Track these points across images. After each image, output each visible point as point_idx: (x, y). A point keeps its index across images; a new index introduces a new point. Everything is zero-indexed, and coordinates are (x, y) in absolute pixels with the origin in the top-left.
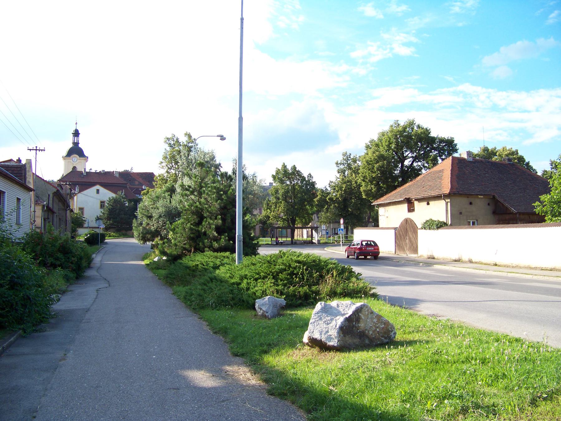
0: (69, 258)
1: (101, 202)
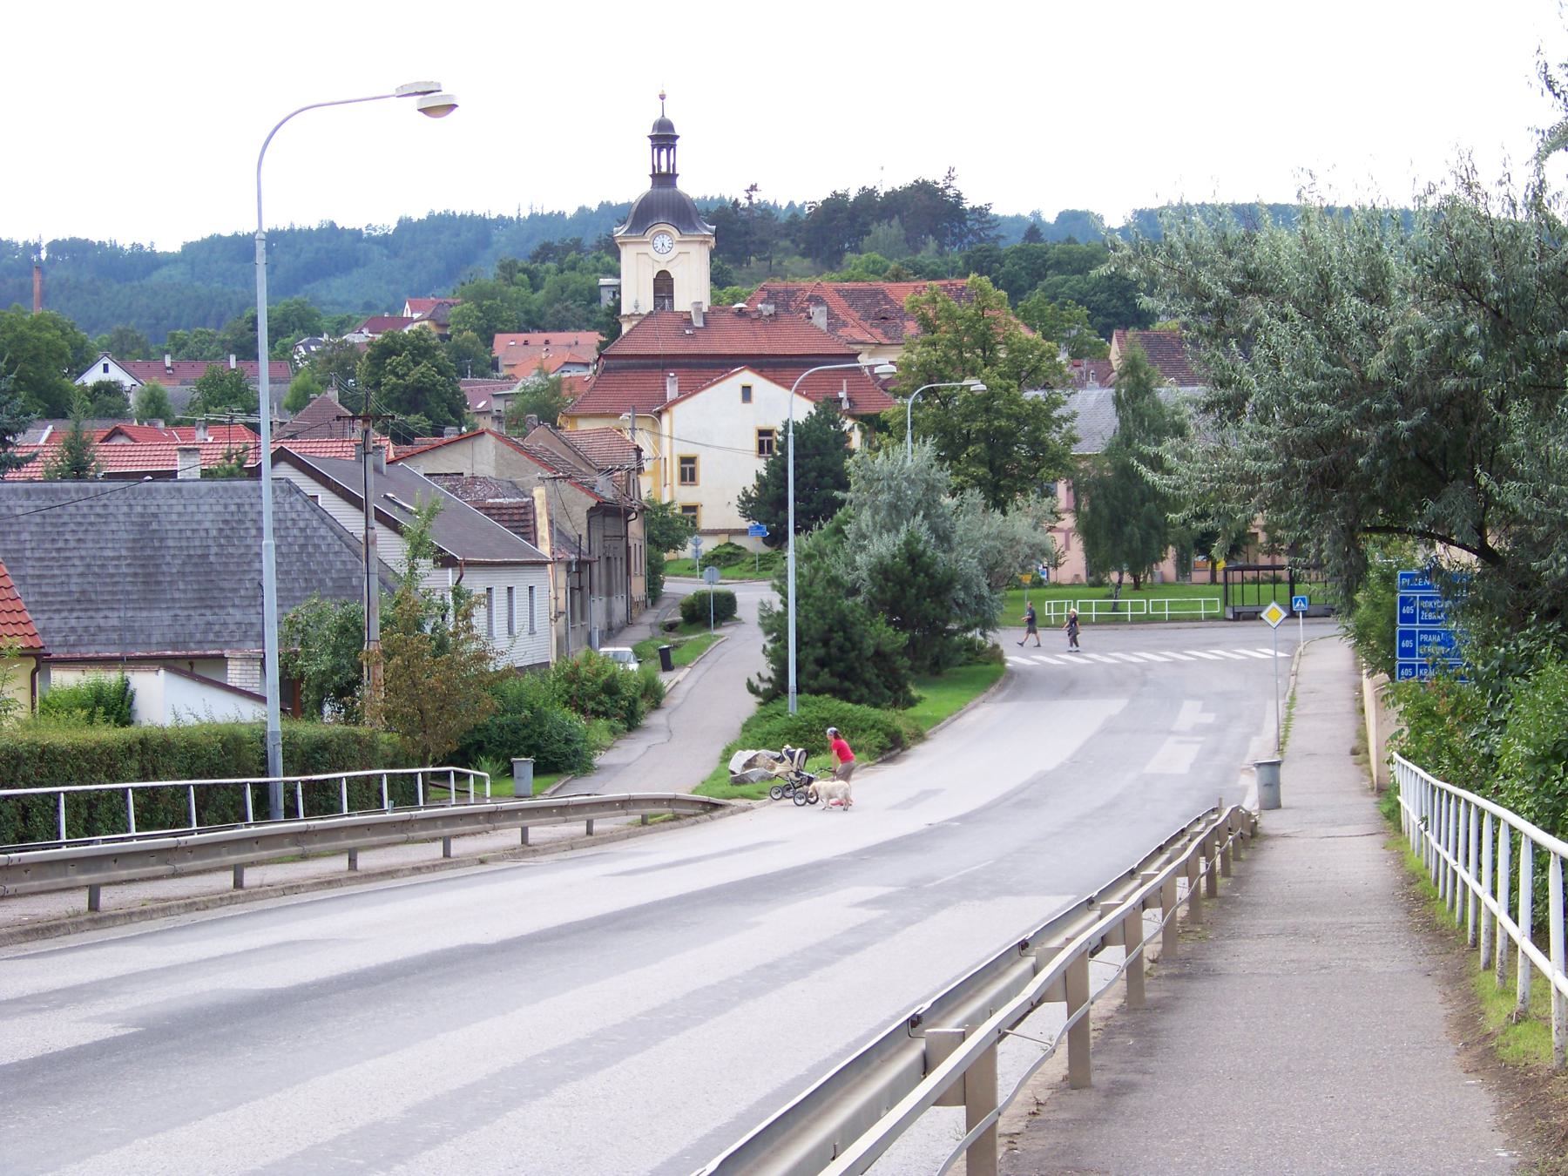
0: (616, 701)
1: (762, 433)
